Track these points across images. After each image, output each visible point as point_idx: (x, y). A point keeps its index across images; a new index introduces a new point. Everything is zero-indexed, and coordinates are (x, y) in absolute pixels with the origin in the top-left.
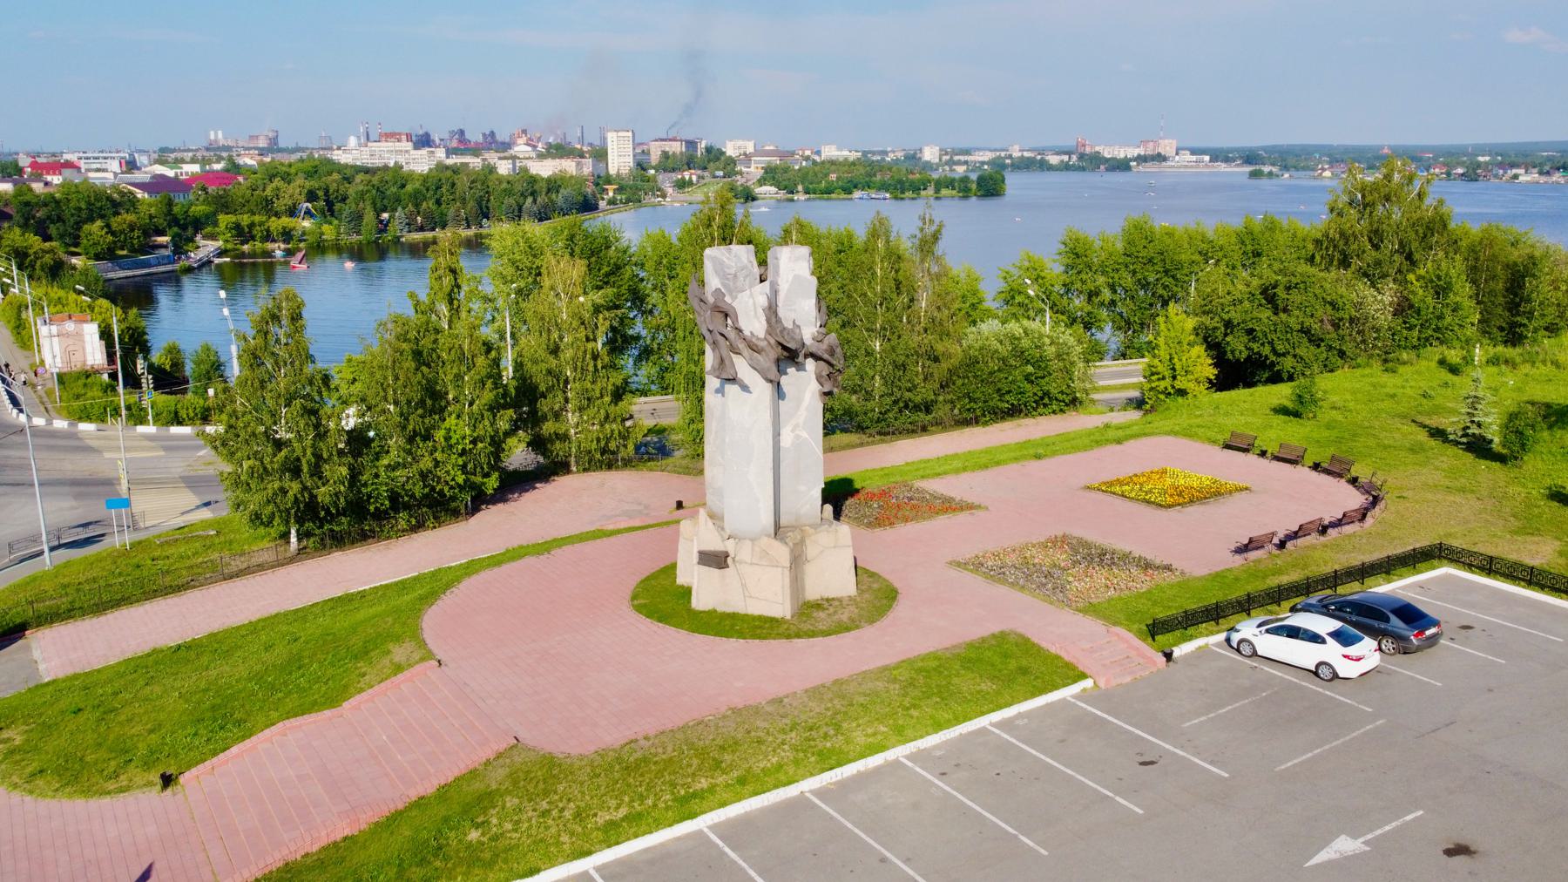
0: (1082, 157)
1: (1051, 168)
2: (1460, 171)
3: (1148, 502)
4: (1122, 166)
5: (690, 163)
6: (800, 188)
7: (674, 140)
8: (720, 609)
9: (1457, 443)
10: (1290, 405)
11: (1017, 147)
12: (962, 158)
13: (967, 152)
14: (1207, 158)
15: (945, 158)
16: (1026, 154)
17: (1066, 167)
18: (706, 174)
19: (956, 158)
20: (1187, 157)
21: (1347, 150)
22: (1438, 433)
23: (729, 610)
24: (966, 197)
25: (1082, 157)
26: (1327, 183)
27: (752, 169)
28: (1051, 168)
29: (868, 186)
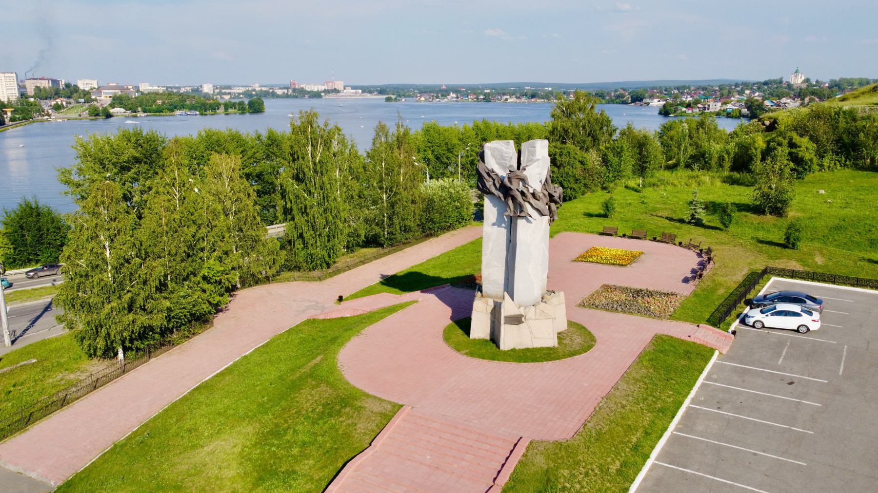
0: (294, 90)
1: (278, 96)
2: (482, 97)
3: (613, 264)
4: (317, 95)
5: (57, 94)
6: (140, 109)
7: (43, 79)
8: (517, 348)
9: (689, 223)
10: (602, 212)
11: (257, 85)
12: (229, 91)
13: (229, 88)
14: (360, 91)
15: (217, 91)
16: (264, 89)
17: (287, 96)
18: (72, 100)
19: (223, 91)
20: (350, 91)
21: (426, 87)
22: (681, 221)
23: (523, 347)
24: (243, 113)
25: (294, 90)
26: (423, 103)
27: (103, 97)
28: (278, 96)
29: (182, 107)
